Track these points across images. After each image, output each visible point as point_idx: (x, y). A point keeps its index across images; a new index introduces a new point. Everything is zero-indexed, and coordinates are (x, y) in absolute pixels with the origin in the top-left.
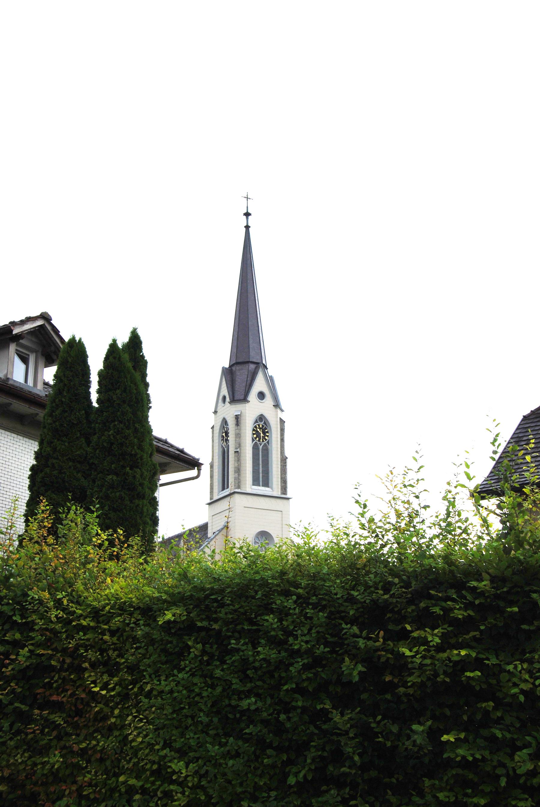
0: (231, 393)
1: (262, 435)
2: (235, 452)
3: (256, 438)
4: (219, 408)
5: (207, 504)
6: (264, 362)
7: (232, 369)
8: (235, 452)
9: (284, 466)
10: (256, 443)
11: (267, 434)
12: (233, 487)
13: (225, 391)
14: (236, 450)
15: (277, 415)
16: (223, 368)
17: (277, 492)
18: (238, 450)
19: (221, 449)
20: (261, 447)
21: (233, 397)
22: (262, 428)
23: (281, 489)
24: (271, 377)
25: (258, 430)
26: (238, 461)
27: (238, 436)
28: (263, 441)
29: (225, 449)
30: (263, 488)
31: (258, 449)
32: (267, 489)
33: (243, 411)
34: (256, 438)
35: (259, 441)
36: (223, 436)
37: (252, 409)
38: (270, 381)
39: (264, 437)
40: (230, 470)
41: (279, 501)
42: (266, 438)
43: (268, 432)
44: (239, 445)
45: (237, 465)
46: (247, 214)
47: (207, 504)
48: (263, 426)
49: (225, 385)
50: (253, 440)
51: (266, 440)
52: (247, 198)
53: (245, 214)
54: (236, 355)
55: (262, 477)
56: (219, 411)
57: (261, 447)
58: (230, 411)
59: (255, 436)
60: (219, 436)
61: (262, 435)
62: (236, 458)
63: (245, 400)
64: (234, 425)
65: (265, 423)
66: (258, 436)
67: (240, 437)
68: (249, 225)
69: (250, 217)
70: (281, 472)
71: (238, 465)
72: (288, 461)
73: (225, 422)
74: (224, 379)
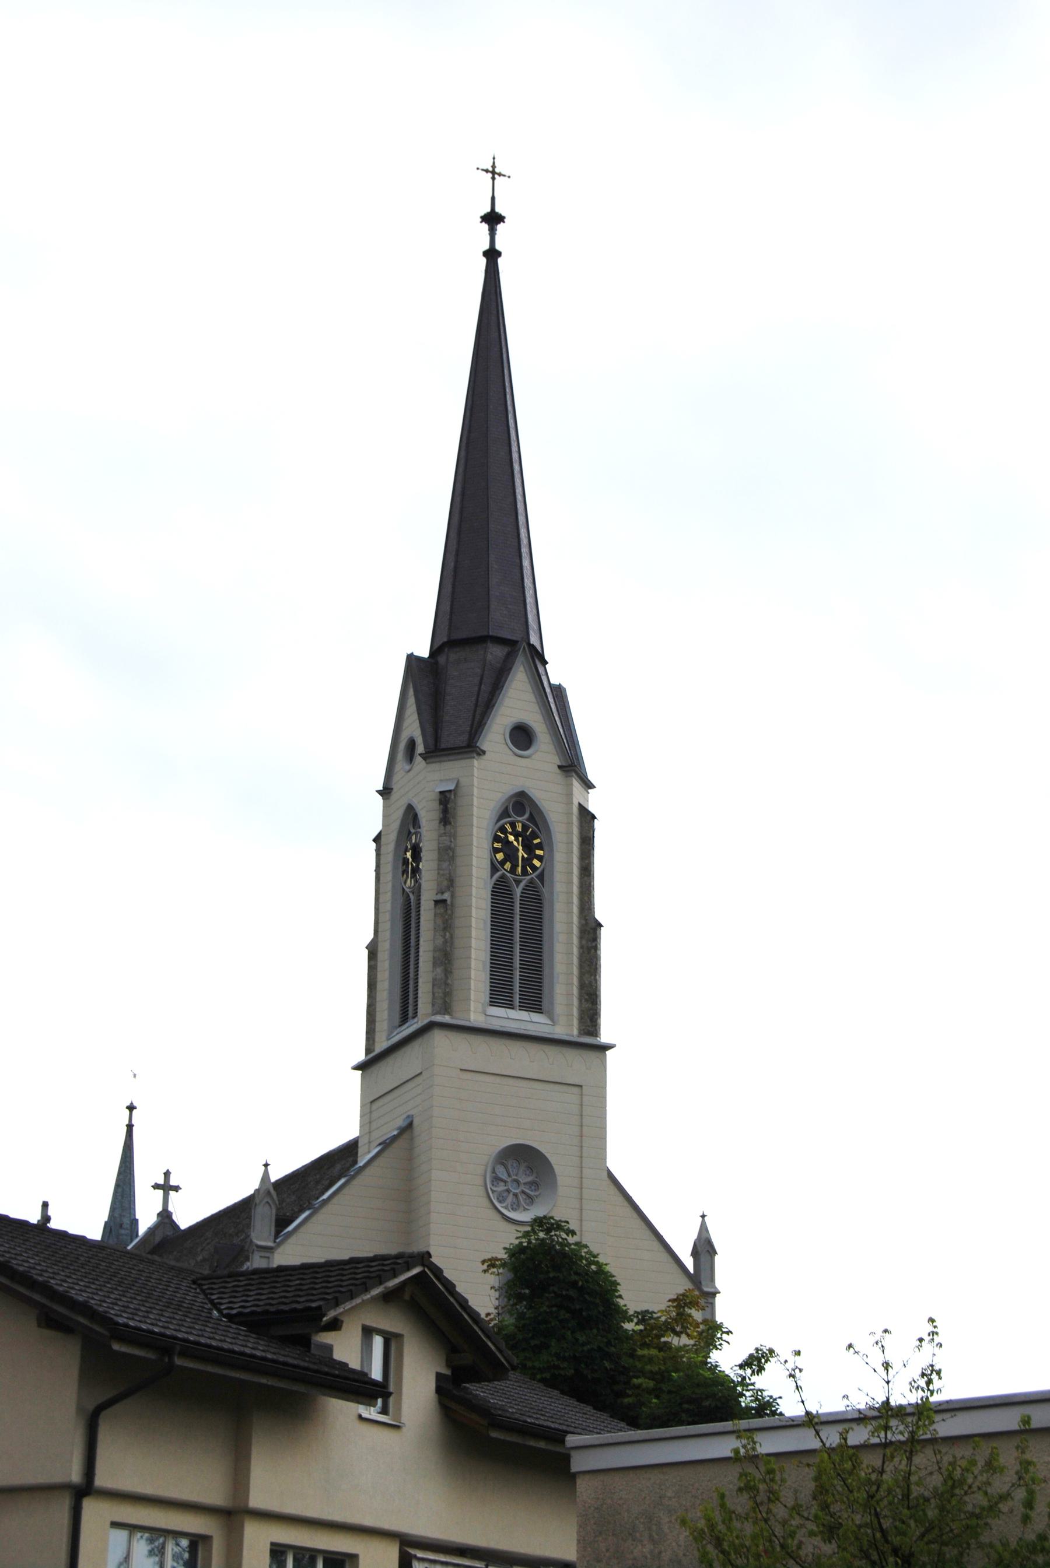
0: (430, 729)
1: (521, 853)
2: (437, 902)
3: (502, 863)
4: (396, 778)
5: (357, 1067)
6: (534, 640)
7: (437, 663)
8: (437, 902)
9: (589, 949)
10: (503, 876)
11: (539, 852)
12: (429, 1009)
13: (413, 729)
14: (439, 897)
15: (570, 795)
16: (411, 659)
17: (567, 1027)
18: (446, 896)
19: (400, 900)
20: (518, 891)
21: (437, 739)
22: (523, 826)
23: (581, 1019)
24: (559, 692)
25: (511, 838)
26: (445, 929)
27: (448, 854)
28: (525, 872)
29: (412, 897)
30: (524, 1015)
31: (510, 894)
32: (535, 1017)
33: (464, 781)
34: (502, 863)
35: (513, 870)
36: (405, 861)
37: (492, 776)
38: (555, 701)
39: (527, 862)
40: (421, 964)
41: (571, 1054)
42: (536, 863)
43: (540, 846)
44: (449, 882)
45: (440, 941)
46: (493, 219)
47: (357, 1067)
48: (525, 827)
49: (415, 716)
50: (494, 869)
51: (534, 868)
52: (493, 173)
53: (485, 219)
54: (451, 620)
55: (520, 975)
56: (395, 787)
57: (518, 891)
58: (428, 780)
59: (500, 856)
60: (395, 860)
61: (521, 853)
62: (439, 922)
63: (470, 748)
64: (435, 824)
65: (531, 818)
66: (510, 854)
67: (452, 859)
68: (498, 247)
69: (500, 227)
70: (581, 967)
71: (446, 942)
72: (605, 934)
73: (411, 817)
74: (411, 692)
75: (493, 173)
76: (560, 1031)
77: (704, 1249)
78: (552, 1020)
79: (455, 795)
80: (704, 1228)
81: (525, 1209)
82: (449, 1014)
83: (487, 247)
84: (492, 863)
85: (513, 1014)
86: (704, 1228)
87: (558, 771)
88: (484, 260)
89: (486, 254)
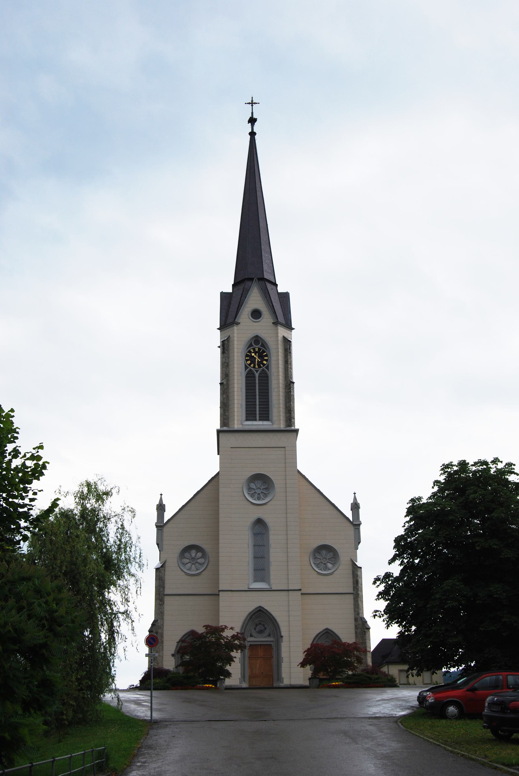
3: (250, 365)
10: (250, 370)
20: (257, 375)
25: (253, 354)
30: (261, 423)
31: (254, 377)
32: (265, 423)
34: (250, 365)
42: (265, 362)
43: (266, 356)
48: (259, 349)
50: (246, 368)
51: (264, 365)
57: (257, 375)
59: (249, 362)
68: (255, 131)
75: (252, 103)
76: (275, 427)
77: (355, 507)
78: (272, 422)
79: (228, 342)
80: (355, 498)
81: (263, 499)
82: (227, 426)
83: (250, 131)
84: (245, 365)
85: (255, 423)
86: (355, 498)
87: (272, 325)
88: (249, 137)
89: (250, 134)
